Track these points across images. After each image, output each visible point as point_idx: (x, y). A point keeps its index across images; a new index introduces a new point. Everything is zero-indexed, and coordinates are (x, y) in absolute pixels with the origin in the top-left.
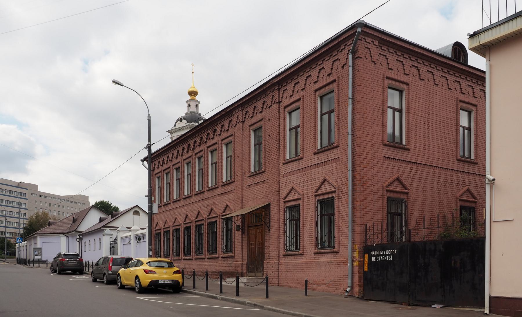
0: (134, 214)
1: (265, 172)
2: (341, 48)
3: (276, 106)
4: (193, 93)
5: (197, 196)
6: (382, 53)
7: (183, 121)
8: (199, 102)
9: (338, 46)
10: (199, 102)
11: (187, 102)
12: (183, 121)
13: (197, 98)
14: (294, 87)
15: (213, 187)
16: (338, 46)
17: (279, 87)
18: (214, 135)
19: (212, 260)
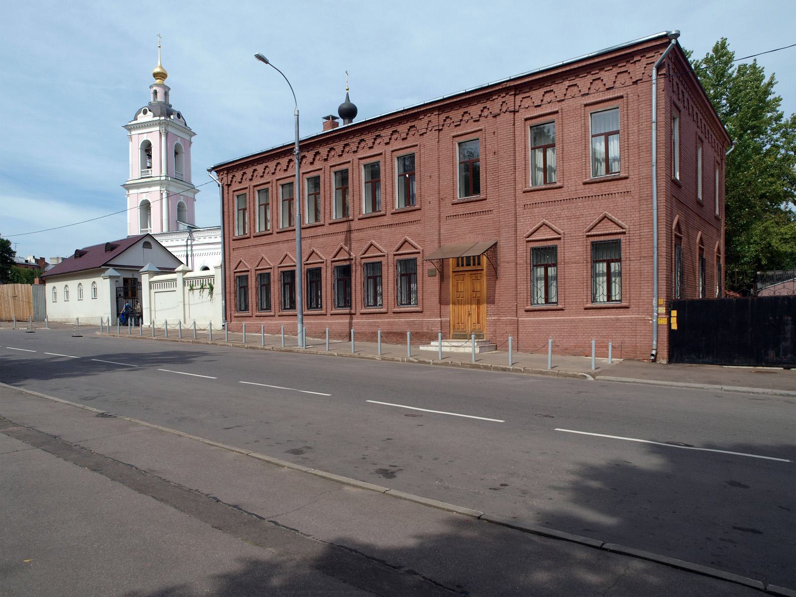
0: (144, 247)
1: (486, 199)
2: (635, 59)
3: (509, 116)
4: (160, 76)
5: (332, 226)
6: (649, 62)
7: (149, 113)
8: (169, 89)
9: (632, 55)
10: (169, 89)
11: (151, 87)
12: (149, 113)
13: (166, 82)
14: (544, 95)
15: (368, 216)
16: (632, 55)
17: (515, 92)
18: (374, 143)
19: (532, 313)
